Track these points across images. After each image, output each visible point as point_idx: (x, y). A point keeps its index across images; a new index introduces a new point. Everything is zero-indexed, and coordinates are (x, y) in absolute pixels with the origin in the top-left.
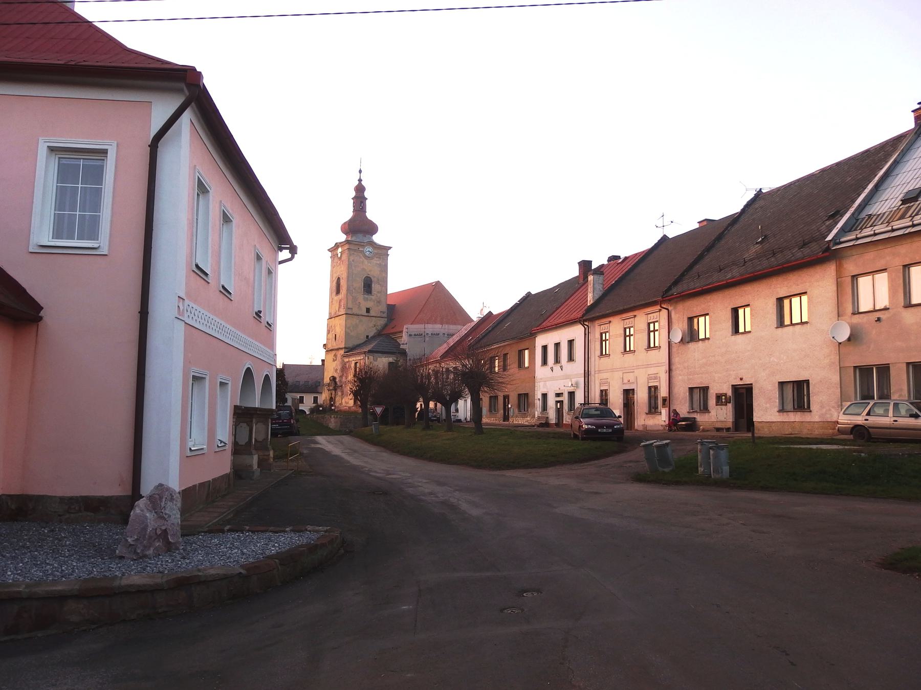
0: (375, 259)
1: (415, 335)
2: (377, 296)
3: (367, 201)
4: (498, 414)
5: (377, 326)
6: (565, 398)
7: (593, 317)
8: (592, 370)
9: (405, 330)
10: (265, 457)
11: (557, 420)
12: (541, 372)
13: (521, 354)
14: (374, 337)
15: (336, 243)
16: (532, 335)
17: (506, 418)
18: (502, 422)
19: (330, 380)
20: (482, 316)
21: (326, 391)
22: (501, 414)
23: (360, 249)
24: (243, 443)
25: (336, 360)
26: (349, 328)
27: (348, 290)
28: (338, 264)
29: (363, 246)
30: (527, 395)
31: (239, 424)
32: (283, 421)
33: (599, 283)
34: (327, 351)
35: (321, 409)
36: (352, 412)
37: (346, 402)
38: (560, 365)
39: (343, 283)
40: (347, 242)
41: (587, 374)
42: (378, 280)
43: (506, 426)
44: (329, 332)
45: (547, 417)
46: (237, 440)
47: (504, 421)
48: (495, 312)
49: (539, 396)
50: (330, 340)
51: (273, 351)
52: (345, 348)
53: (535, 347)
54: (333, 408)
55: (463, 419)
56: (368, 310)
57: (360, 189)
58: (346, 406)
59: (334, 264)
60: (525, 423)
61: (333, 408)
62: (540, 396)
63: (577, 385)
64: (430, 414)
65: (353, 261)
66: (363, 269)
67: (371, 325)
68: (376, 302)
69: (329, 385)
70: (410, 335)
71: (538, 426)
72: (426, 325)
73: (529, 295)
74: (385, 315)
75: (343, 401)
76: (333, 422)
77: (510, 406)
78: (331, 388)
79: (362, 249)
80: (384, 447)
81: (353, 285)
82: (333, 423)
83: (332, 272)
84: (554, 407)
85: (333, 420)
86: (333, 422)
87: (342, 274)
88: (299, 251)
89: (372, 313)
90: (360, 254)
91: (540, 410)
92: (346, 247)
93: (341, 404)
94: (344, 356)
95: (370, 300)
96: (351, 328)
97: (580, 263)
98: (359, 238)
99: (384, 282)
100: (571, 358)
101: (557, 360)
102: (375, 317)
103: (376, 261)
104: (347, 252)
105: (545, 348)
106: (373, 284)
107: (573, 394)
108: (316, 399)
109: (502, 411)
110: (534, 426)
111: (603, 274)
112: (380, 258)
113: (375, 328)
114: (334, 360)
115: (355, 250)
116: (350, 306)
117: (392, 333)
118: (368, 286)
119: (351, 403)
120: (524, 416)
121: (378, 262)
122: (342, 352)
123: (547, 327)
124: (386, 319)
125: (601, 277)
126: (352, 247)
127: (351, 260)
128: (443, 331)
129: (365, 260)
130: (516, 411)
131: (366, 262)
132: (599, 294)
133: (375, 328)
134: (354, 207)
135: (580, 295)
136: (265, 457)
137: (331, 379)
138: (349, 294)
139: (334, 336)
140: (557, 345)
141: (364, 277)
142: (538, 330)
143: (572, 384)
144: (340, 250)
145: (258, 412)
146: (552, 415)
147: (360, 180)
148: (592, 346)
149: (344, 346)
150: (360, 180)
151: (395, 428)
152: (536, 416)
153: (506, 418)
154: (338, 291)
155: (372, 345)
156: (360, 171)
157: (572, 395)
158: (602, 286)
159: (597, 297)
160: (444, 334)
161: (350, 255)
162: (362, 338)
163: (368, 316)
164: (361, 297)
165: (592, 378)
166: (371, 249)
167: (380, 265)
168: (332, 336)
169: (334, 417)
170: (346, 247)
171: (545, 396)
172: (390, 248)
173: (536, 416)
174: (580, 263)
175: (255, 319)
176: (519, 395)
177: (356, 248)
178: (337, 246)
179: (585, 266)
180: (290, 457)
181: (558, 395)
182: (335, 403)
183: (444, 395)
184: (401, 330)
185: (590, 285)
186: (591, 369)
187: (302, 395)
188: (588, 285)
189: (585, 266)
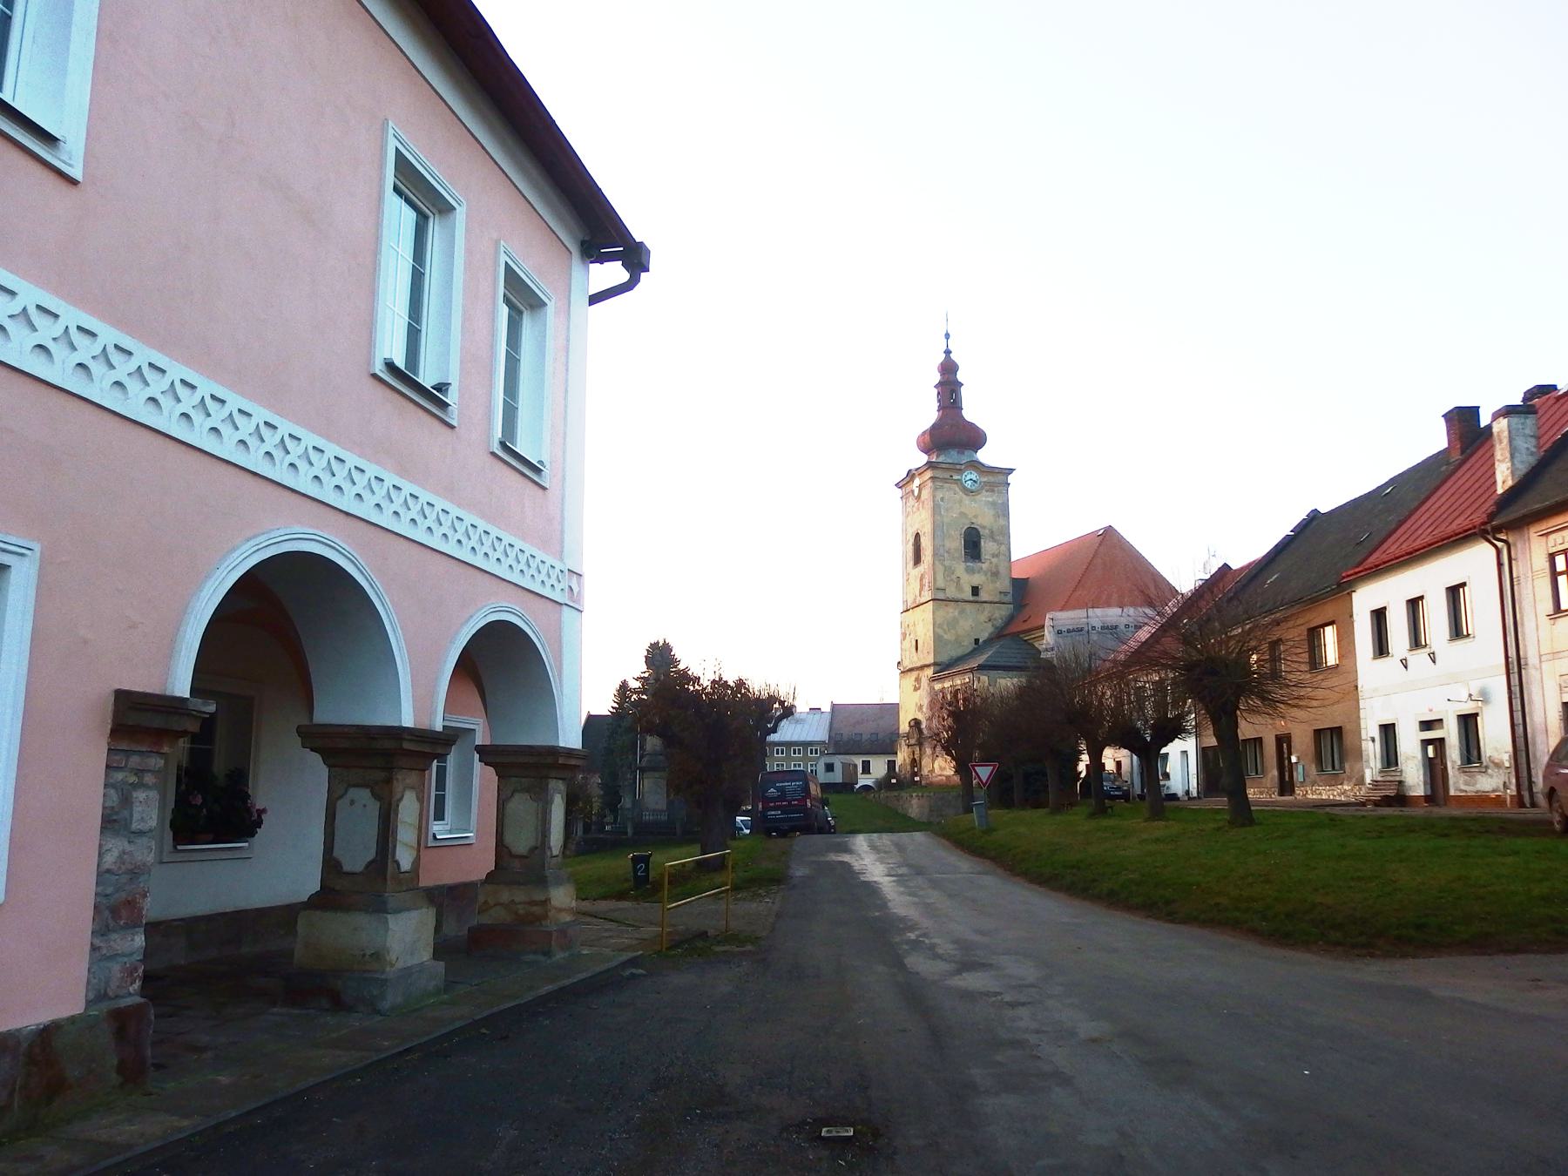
0: (984, 493)
1: (1069, 631)
2: (991, 563)
3: (963, 389)
4: (1264, 780)
5: (995, 619)
6: (1451, 733)
7: (1525, 516)
8: (1530, 652)
9: (1048, 623)
10: (535, 909)
11: (1429, 787)
12: (1370, 671)
13: (1314, 635)
14: (990, 641)
15: (910, 470)
16: (1343, 588)
17: (1286, 786)
18: (1275, 797)
19: (910, 727)
20: (1208, 577)
21: (904, 748)
22: (1272, 778)
23: (955, 477)
24: (359, 866)
25: (919, 688)
26: (940, 626)
27: (935, 555)
28: (915, 509)
29: (960, 471)
30: (1337, 732)
31: (346, 791)
32: (790, 802)
33: (1524, 435)
34: (902, 672)
35: (894, 781)
36: (953, 786)
37: (940, 768)
38: (1427, 650)
39: (926, 543)
40: (930, 465)
41: (1515, 667)
42: (992, 532)
43: (1285, 804)
44: (904, 636)
45: (1401, 782)
46: (337, 853)
47: (1281, 794)
48: (1235, 565)
49: (1370, 729)
50: (908, 653)
51: (560, 555)
52: (935, 664)
53: (1351, 616)
54: (917, 779)
55: (1180, 793)
56: (975, 591)
57: (949, 369)
58: (940, 775)
59: (909, 509)
60: (1338, 798)
61: (917, 779)
62: (1375, 732)
63: (1484, 697)
64: (1104, 783)
65: (942, 499)
66: (963, 514)
67: (983, 617)
68: (989, 574)
69: (908, 736)
70: (1059, 632)
71: (1376, 804)
72: (1090, 610)
73: (1314, 516)
74: (1009, 598)
75: (936, 765)
76: (915, 806)
77: (1294, 759)
78: (913, 741)
79: (959, 477)
80: (993, 859)
81: (944, 546)
82: (915, 806)
83: (904, 523)
84: (1419, 756)
85: (915, 801)
86: (915, 806)
87: (923, 526)
88: (654, 263)
89: (984, 596)
90: (955, 487)
91: (1379, 765)
92: (929, 474)
93: (933, 771)
94: (933, 680)
95: (979, 572)
96: (945, 627)
97: (1448, 417)
98: (952, 456)
99: (1003, 535)
100: (1457, 631)
101: (1416, 642)
102: (991, 603)
103: (985, 497)
104: (930, 484)
105: (1379, 616)
106: (982, 541)
107: (1471, 722)
108: (891, 764)
109: (1275, 773)
110: (1363, 804)
111: (1535, 412)
112: (993, 491)
113: (990, 624)
114: (916, 689)
115: (945, 480)
116: (941, 584)
117: (1025, 632)
118: (972, 544)
119: (950, 772)
120: (1335, 780)
121: (990, 499)
122: (929, 672)
123: (1384, 563)
124: (1012, 606)
125: (1530, 421)
126: (939, 474)
127: (938, 498)
128: (1124, 621)
129: (964, 496)
130: (1313, 770)
131: (966, 500)
132: (1526, 462)
133: (990, 624)
134: (939, 401)
135: (1460, 482)
136: (535, 909)
137: (912, 723)
138: (937, 562)
139: (914, 643)
140: (1414, 604)
141: (966, 527)
142: (1356, 573)
143: (1470, 695)
144: (917, 482)
145: (406, 745)
146: (1413, 776)
147: (948, 352)
148: (1525, 593)
149: (930, 660)
150: (948, 352)
151: (1029, 814)
152: (1368, 780)
153: (1286, 786)
154: (917, 559)
155: (986, 656)
156: (947, 336)
157: (1468, 723)
158: (1533, 441)
159: (1523, 469)
160: (1127, 626)
161: (935, 489)
162: (965, 644)
163: (977, 602)
164: (960, 568)
165: (1531, 674)
166: (974, 476)
167: (994, 504)
168: (909, 643)
169: (917, 796)
170: (929, 474)
171: (1388, 731)
172: (1012, 470)
173: (1368, 780)
174: (1448, 417)
175: (376, 383)
176: (1318, 733)
177: (947, 475)
178: (911, 475)
179: (1463, 422)
180: (670, 903)
181: (1427, 725)
182: (920, 769)
183: (1138, 730)
184: (1040, 623)
185: (1501, 442)
186: (1526, 652)
187: (866, 758)
188: (1493, 446)
189: (1463, 422)
